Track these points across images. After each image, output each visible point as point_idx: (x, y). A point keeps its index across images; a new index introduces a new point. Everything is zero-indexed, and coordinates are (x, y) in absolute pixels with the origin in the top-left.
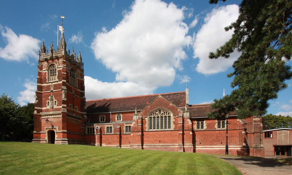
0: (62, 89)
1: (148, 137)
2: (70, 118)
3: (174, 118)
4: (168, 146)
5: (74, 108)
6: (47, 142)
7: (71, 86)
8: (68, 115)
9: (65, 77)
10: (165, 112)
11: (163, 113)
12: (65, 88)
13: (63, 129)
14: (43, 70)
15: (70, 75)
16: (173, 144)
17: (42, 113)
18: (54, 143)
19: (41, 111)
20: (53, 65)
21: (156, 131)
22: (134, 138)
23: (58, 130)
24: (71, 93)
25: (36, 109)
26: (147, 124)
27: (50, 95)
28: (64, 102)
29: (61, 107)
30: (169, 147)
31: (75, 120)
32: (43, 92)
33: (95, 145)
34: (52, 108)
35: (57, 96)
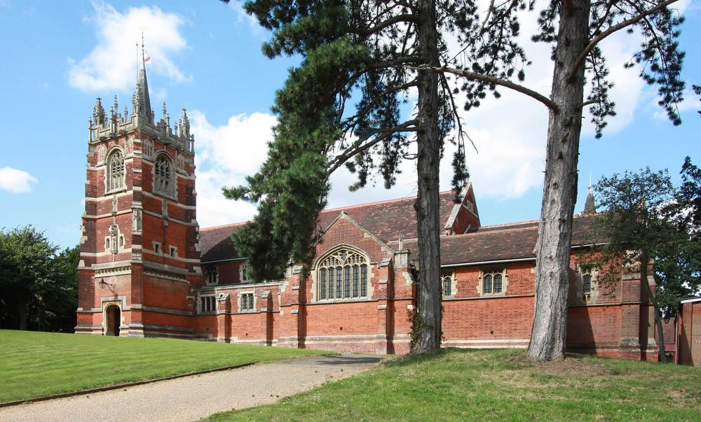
0: (133, 209)
1: (316, 318)
2: (153, 275)
3: (373, 269)
4: (359, 339)
5: (165, 251)
6: (105, 333)
7: (157, 198)
8: (146, 269)
9: (140, 179)
10: (353, 256)
11: (349, 259)
12: (138, 205)
13: (133, 301)
14: (99, 163)
15: (157, 170)
16: (370, 336)
17: (97, 265)
18: (117, 334)
19: (94, 260)
20: (116, 151)
21: (334, 303)
22: (287, 322)
23: (125, 305)
24: (156, 215)
25: (83, 258)
26: (314, 286)
27: (111, 223)
28: (136, 239)
29: (130, 250)
30: (360, 342)
31: (169, 280)
32: (97, 217)
33: (216, 341)
34: (115, 254)
35: (125, 224)
